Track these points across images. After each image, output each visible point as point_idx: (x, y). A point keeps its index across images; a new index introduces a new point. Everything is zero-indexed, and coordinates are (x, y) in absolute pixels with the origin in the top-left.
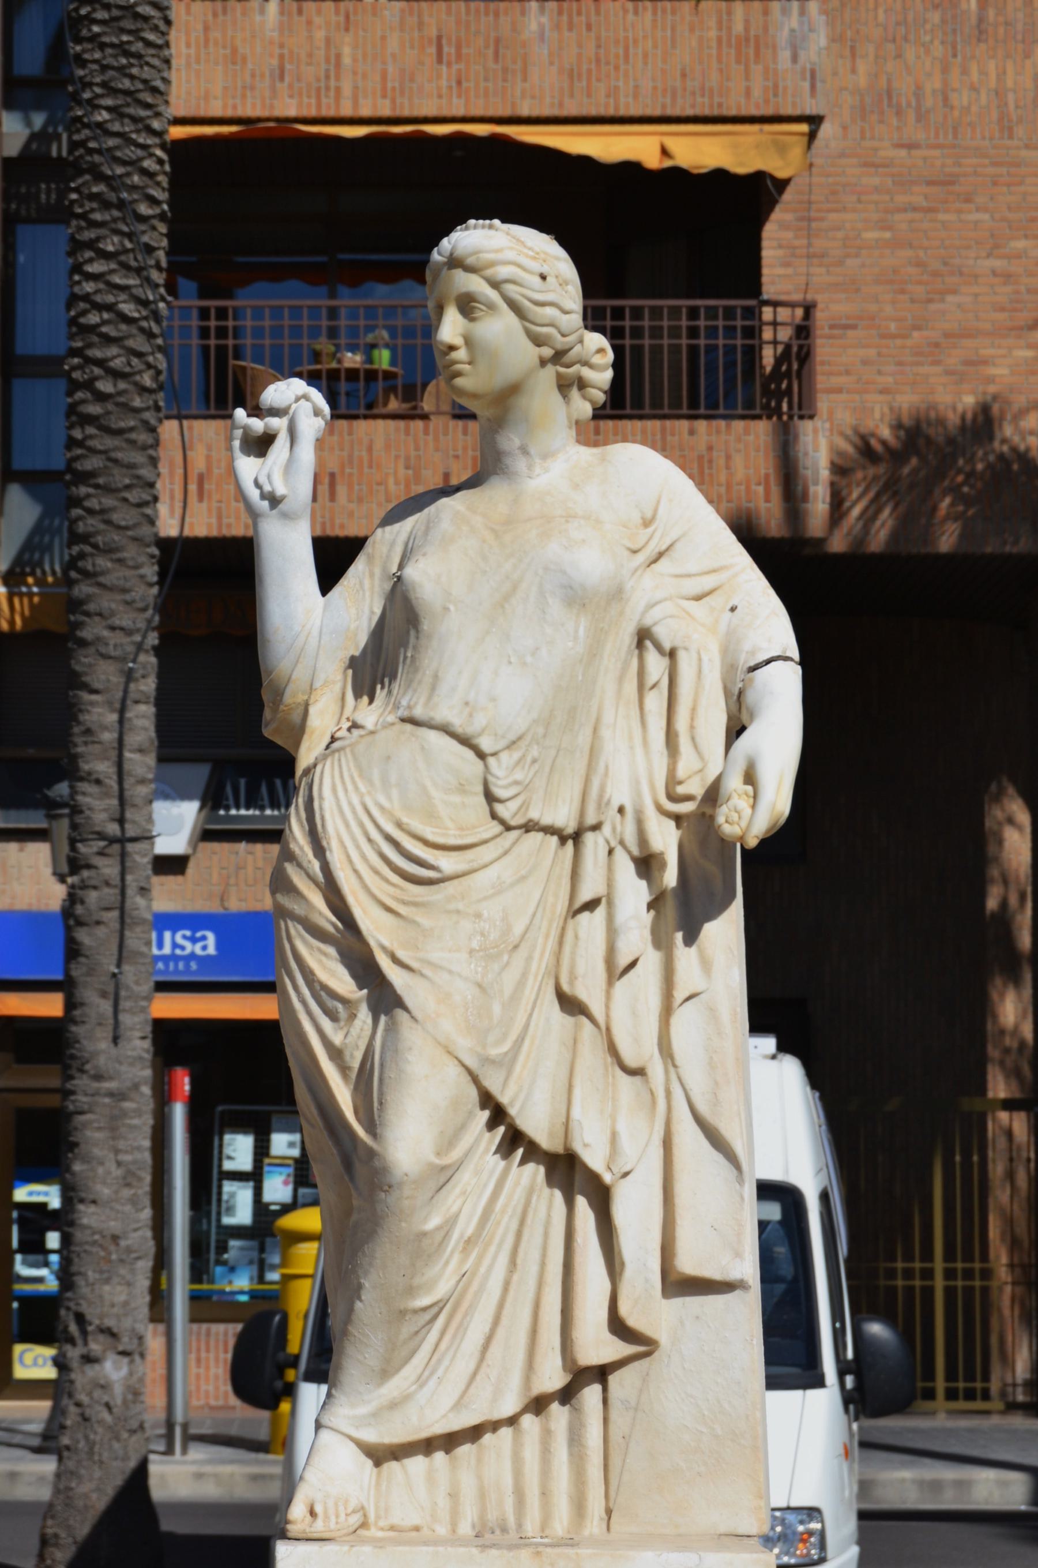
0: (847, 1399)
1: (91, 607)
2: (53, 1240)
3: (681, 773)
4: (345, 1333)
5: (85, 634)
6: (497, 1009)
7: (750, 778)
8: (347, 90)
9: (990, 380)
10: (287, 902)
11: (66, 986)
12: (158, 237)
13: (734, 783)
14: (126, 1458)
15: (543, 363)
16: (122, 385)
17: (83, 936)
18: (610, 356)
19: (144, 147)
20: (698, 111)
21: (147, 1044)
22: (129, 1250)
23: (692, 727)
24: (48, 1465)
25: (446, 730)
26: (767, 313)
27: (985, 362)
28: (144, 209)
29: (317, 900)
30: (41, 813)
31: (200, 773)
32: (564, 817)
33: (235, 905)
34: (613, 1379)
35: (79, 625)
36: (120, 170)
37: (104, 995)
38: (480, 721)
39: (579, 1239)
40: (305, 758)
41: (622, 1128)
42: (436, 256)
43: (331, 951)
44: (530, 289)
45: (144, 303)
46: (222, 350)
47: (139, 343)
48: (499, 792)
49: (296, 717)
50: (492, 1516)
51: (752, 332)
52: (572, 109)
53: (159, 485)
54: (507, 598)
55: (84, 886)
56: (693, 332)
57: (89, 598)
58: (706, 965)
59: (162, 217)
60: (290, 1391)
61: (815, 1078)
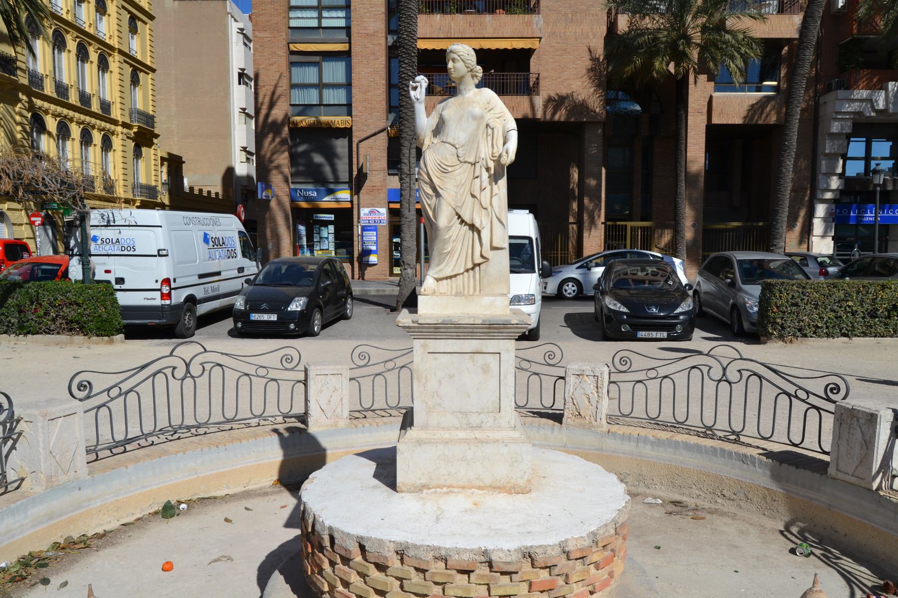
3: (494, 152)
5: (402, 136)
7: (507, 153)
10: (420, 177)
11: (400, 202)
12: (415, 60)
13: (504, 154)
15: (468, 72)
17: (403, 192)
18: (482, 71)
23: (496, 143)
24: (398, 288)
25: (450, 144)
26: (531, 75)
27: (571, 85)
28: (413, 54)
29: (426, 176)
32: (472, 160)
34: (481, 266)
38: (456, 142)
39: (475, 240)
40: (423, 150)
41: (483, 219)
44: (466, 57)
45: (413, 73)
48: (459, 155)
49: (422, 142)
50: (459, 291)
52: (494, 36)
54: (461, 118)
56: (517, 79)
57: (403, 129)
58: (499, 189)
59: (416, 56)
61: (536, 218)
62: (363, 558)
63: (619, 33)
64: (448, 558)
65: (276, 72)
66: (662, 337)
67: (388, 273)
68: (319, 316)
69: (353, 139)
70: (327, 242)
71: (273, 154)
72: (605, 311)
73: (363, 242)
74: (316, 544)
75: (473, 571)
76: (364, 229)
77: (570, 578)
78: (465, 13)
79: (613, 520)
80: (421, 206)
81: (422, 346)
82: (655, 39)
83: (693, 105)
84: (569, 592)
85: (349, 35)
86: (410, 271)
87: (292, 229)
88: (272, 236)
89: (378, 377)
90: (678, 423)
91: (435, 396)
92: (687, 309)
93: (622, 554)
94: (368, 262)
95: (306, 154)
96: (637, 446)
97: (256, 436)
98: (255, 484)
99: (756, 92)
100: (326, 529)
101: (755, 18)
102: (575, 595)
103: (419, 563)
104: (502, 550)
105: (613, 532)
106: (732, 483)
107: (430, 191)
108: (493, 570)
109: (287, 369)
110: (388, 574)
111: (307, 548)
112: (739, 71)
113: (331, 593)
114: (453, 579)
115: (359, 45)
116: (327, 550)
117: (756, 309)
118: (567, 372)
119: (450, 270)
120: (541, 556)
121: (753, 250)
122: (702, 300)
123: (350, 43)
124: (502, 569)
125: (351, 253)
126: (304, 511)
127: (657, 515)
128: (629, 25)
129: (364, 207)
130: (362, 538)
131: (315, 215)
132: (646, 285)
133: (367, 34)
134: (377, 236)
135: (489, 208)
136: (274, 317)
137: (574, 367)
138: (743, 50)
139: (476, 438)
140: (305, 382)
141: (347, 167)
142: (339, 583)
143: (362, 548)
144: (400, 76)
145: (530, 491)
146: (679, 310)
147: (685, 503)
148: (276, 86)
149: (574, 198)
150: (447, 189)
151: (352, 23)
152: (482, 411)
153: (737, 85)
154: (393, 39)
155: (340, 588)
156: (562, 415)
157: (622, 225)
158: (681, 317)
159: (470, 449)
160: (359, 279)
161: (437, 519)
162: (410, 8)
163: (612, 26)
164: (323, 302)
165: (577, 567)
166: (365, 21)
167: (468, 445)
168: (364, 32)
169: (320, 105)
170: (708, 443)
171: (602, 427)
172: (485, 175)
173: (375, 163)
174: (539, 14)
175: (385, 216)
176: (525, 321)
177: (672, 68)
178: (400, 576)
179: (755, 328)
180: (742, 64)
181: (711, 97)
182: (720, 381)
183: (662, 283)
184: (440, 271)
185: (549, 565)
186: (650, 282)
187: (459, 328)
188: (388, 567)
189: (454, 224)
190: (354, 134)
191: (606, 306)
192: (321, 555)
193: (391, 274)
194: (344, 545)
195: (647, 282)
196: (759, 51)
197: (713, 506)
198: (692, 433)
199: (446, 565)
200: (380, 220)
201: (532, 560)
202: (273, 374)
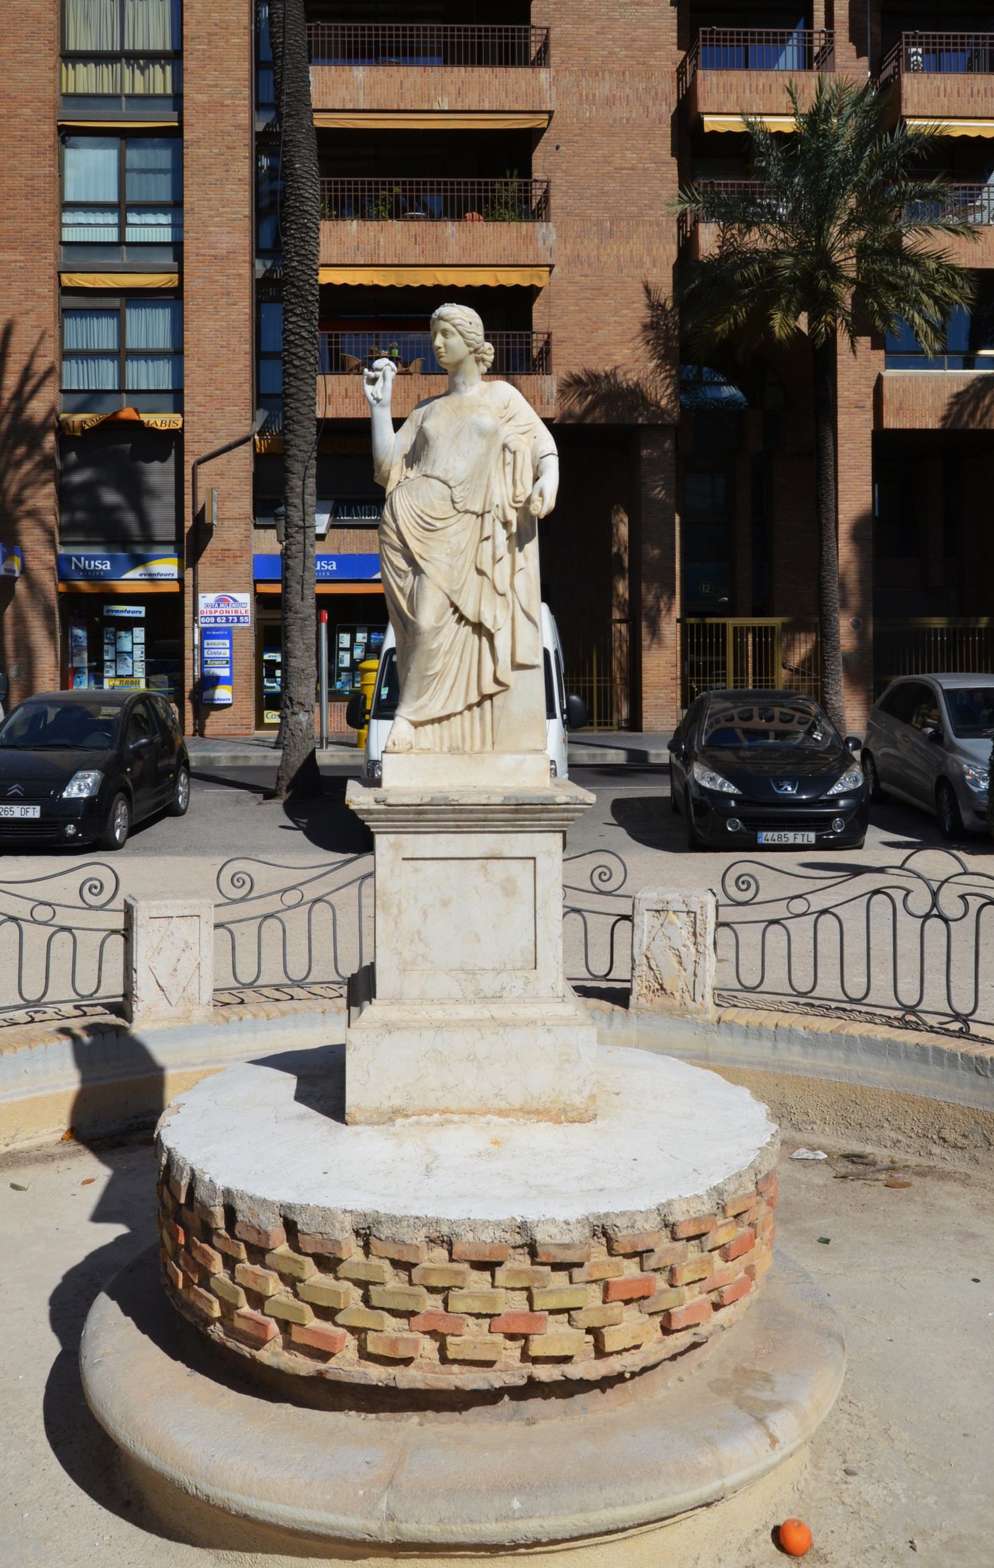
0: (564, 723)
1: (293, 443)
2: (278, 673)
3: (518, 493)
4: (404, 684)
5: (290, 453)
6: (456, 574)
7: (541, 495)
8: (382, 254)
9: (615, 361)
12: (315, 308)
13: (536, 497)
14: (307, 748)
15: (471, 353)
16: (303, 362)
17: (290, 562)
18: (493, 350)
19: (310, 275)
20: (509, 263)
21: (314, 601)
22: (308, 674)
24: (279, 753)
26: (534, 336)
28: (310, 298)
29: (394, 537)
30: (272, 519)
31: (330, 504)
32: (478, 508)
33: (343, 552)
34: (495, 699)
35: (288, 450)
36: (301, 284)
37: (298, 583)
40: (389, 488)
41: (498, 613)
42: (434, 316)
43: (399, 554)
44: (466, 327)
45: (311, 332)
46: (337, 349)
47: (309, 347)
49: (386, 475)
51: (528, 343)
53: (317, 398)
55: (290, 544)
56: (508, 343)
57: (292, 440)
58: (526, 558)
59: (317, 301)
60: (368, 722)
62: (290, 1247)
63: (701, 258)
64: (454, 1239)
65: (32, 327)
66: (805, 842)
67: (253, 723)
68: (124, 807)
69: (186, 458)
70: (129, 661)
71: (23, 487)
72: (694, 792)
73: (204, 662)
74: (197, 1224)
75: (500, 1264)
76: (206, 634)
77: (678, 1276)
78: (405, 219)
79: (751, 1167)
80: (384, 587)
81: (391, 846)
82: (771, 270)
83: (846, 393)
84: (677, 1303)
85: (179, 256)
86: (303, 717)
87: (59, 635)
88: (17, 650)
89: (270, 921)
90: (852, 1001)
91: (417, 941)
92: (852, 786)
93: (767, 1235)
94: (213, 700)
95: (89, 488)
96: (775, 1047)
97: (30, 1041)
98: (28, 1139)
99: (964, 369)
100: (219, 1193)
101: (956, 232)
102: (687, 1309)
103: (400, 1252)
104: (553, 1221)
105: (751, 1188)
106: (959, 1115)
107: (402, 564)
108: (538, 1260)
109: (91, 908)
110: (340, 1275)
111: (174, 1237)
112: (932, 329)
113: (226, 1322)
114: (464, 1280)
115: (199, 277)
116: (220, 1236)
117: (984, 785)
118: (637, 905)
119: (439, 706)
120: (625, 1232)
121: (974, 671)
122: (879, 769)
123: (181, 273)
124: (554, 1257)
125: (178, 683)
126: (169, 1167)
127: (819, 1181)
128: (719, 244)
129: (205, 591)
130: (290, 1207)
131: (106, 608)
132: (771, 741)
133: (215, 257)
134: (231, 648)
135: (509, 594)
136: (34, 812)
137: (649, 895)
138: (939, 289)
139: (493, 1018)
140: (127, 933)
141: (172, 513)
142: (243, 1299)
143: (290, 1227)
144: (285, 339)
145: (595, 1116)
146: (837, 789)
147: (871, 1157)
148: (33, 355)
149: (621, 571)
150: (433, 558)
151: (185, 235)
152: (502, 967)
153: (930, 355)
154: (265, 266)
155: (246, 1309)
156: (628, 992)
157: (717, 625)
158: (842, 803)
159: (483, 1038)
160: (194, 735)
161: (428, 1171)
162: (306, 211)
163: (687, 245)
164: (132, 780)
165: (690, 1255)
166: (211, 233)
167: (479, 1030)
168: (207, 251)
169: (121, 391)
170: (911, 1037)
171: (706, 1012)
172: (501, 535)
173: (228, 504)
174: (548, 220)
175: (249, 608)
176: (581, 798)
177: (803, 322)
178: (363, 1278)
179: (985, 823)
180: (939, 315)
181: (880, 379)
182: (927, 917)
183: (801, 736)
184: (421, 708)
185: (640, 1249)
186: (780, 735)
187: (461, 812)
188: (340, 1261)
189: (446, 623)
190: (188, 447)
191: (696, 782)
192: (206, 1246)
193: (260, 724)
194: (254, 1222)
195: (772, 734)
196: (968, 291)
197: (925, 1162)
198: (877, 1021)
199: (450, 1253)
200: (238, 617)
201: (609, 1241)
202: (64, 917)
